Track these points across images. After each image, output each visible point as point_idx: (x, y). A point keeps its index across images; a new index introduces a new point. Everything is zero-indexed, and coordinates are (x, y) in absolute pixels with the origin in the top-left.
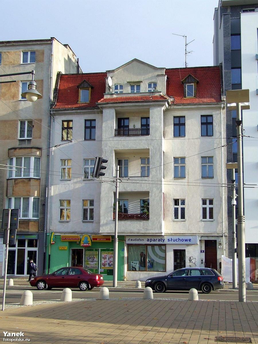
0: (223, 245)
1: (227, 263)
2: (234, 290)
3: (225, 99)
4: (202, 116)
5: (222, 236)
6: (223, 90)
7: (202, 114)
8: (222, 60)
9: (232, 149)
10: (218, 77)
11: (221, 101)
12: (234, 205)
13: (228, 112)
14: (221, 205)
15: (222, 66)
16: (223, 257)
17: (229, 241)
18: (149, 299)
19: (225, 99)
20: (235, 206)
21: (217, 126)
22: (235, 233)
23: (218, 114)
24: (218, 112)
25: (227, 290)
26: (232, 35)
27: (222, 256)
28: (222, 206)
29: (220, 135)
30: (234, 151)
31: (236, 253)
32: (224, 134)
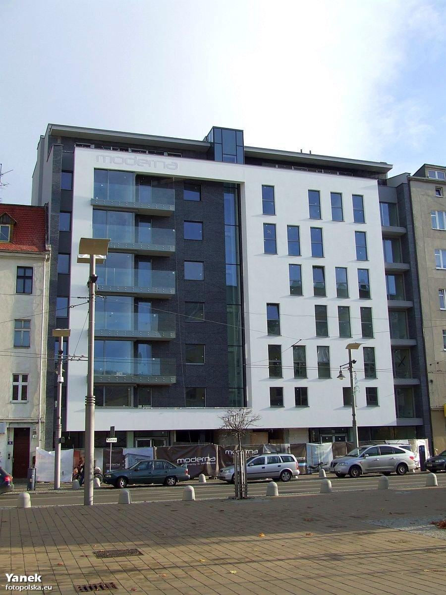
0: (39, 433)
1: (43, 457)
2: (57, 491)
3: (50, 249)
4: (314, 267)
5: (38, 423)
6: (48, 237)
7: (315, 264)
8: (47, 199)
9: (55, 312)
10: (42, 220)
11: (45, 250)
12: (60, 382)
13: (53, 266)
14: (38, 382)
15: (47, 208)
16: (38, 449)
17: (46, 429)
18: (191, 500)
19: (50, 249)
20: (61, 384)
21: (38, 281)
22: (60, 418)
23: (40, 267)
24: (40, 264)
25: (48, 491)
26: (63, 171)
27: (37, 448)
28: (39, 385)
29: (41, 294)
30: (61, 314)
31: (60, 444)
32: (46, 292)
